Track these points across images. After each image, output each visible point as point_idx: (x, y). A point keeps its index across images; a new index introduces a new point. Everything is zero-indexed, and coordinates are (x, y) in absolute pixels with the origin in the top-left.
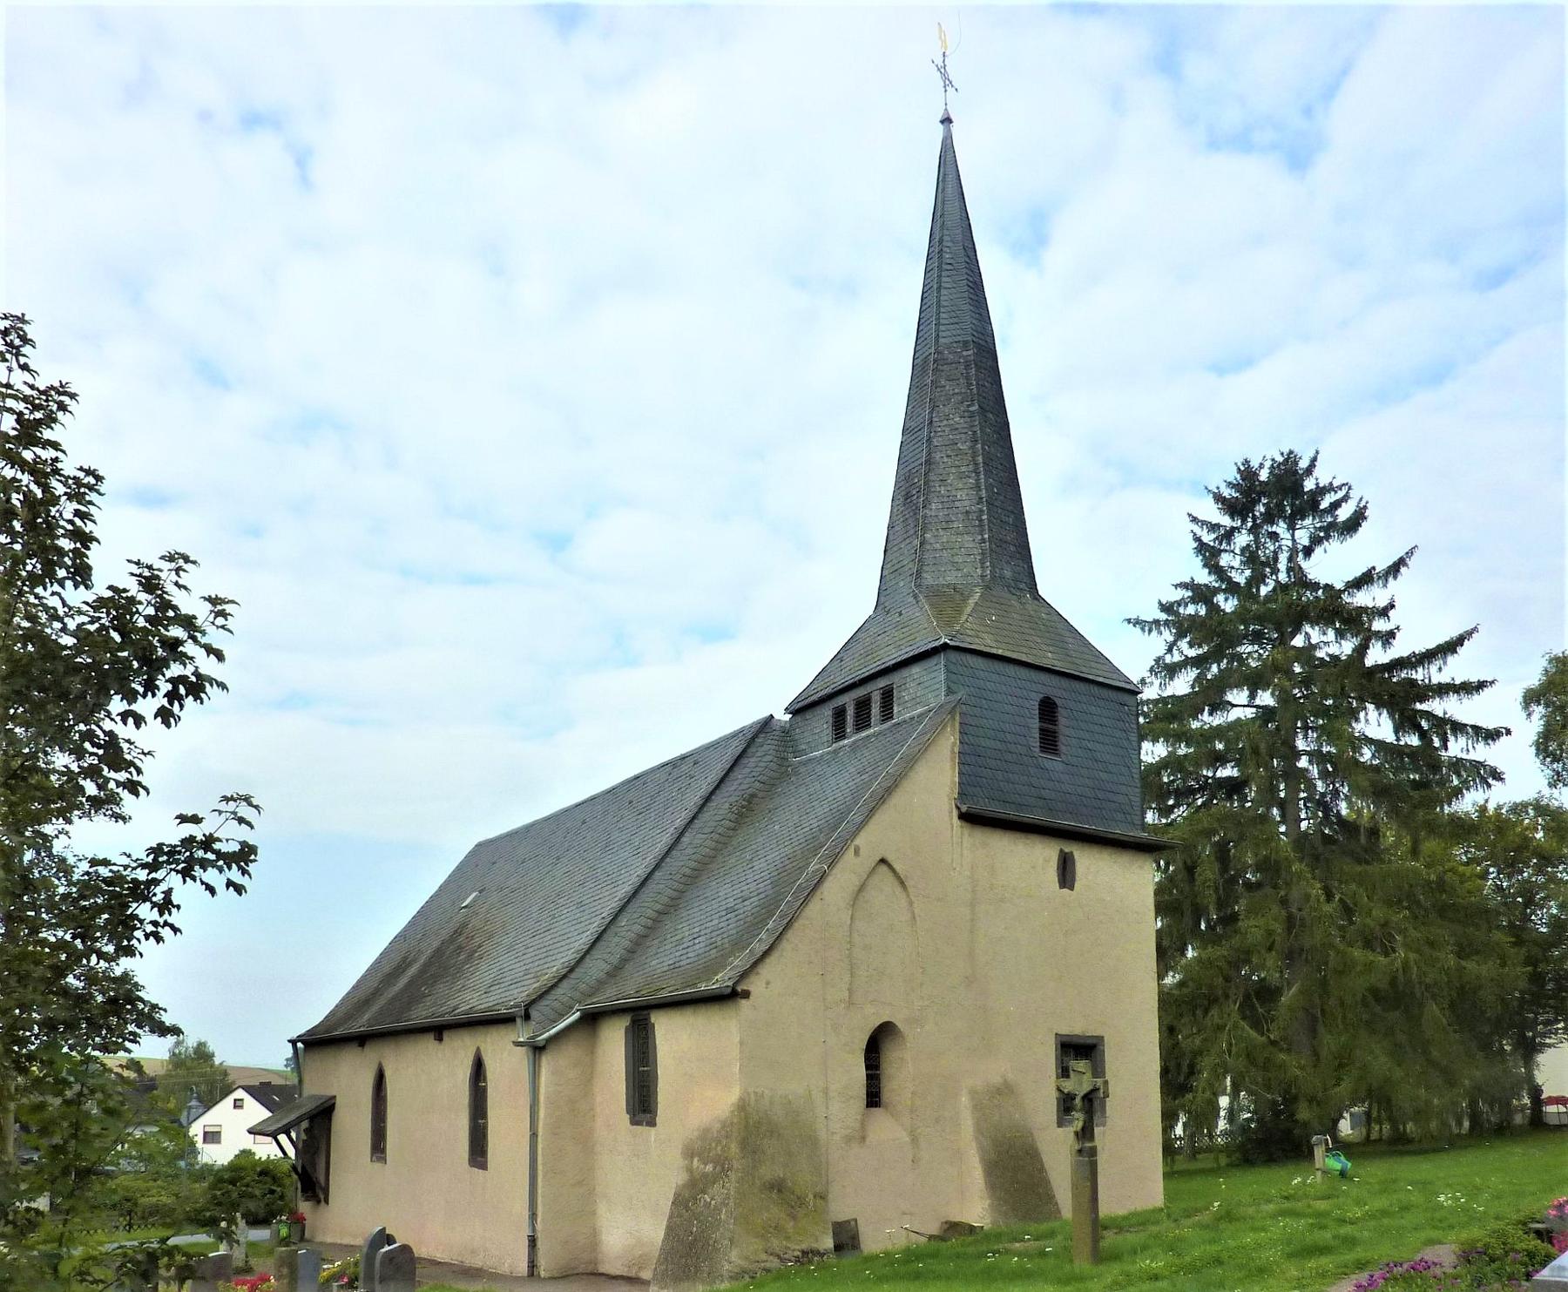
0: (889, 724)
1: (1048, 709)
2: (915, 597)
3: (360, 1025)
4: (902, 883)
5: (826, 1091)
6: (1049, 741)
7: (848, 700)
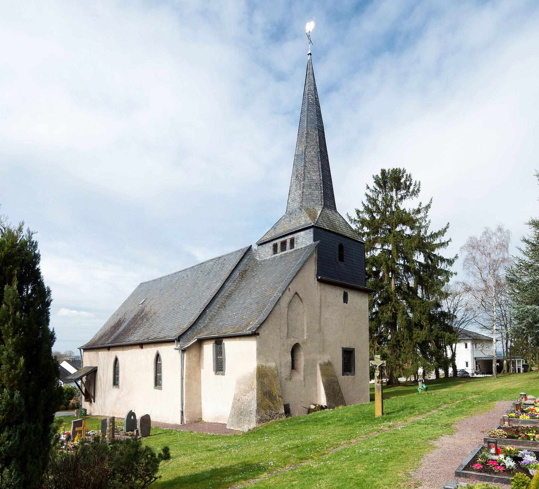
0: (293, 250)
1: (341, 247)
2: (301, 209)
3: (107, 344)
4: (301, 300)
5: (280, 364)
6: (341, 258)
7: (278, 241)
